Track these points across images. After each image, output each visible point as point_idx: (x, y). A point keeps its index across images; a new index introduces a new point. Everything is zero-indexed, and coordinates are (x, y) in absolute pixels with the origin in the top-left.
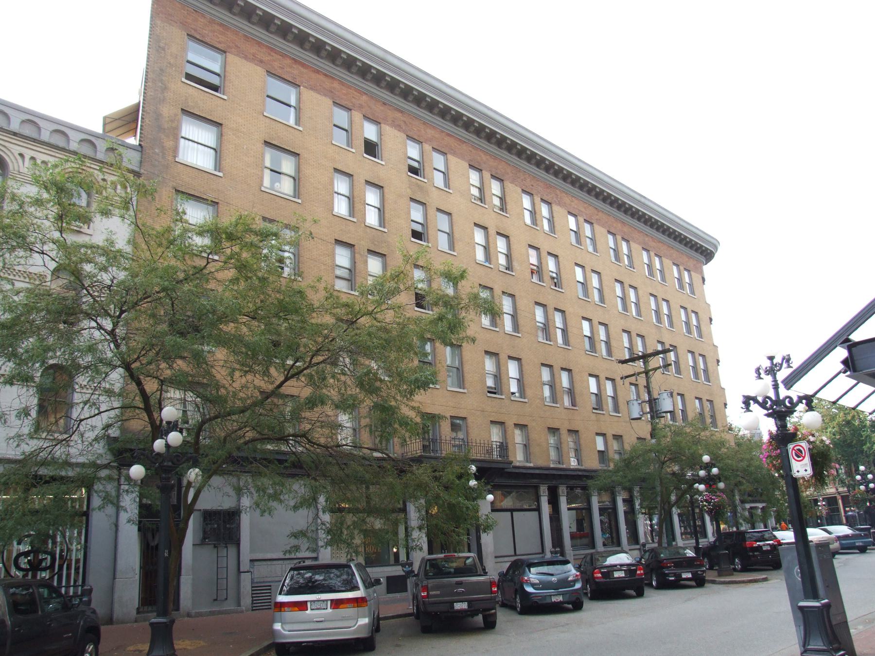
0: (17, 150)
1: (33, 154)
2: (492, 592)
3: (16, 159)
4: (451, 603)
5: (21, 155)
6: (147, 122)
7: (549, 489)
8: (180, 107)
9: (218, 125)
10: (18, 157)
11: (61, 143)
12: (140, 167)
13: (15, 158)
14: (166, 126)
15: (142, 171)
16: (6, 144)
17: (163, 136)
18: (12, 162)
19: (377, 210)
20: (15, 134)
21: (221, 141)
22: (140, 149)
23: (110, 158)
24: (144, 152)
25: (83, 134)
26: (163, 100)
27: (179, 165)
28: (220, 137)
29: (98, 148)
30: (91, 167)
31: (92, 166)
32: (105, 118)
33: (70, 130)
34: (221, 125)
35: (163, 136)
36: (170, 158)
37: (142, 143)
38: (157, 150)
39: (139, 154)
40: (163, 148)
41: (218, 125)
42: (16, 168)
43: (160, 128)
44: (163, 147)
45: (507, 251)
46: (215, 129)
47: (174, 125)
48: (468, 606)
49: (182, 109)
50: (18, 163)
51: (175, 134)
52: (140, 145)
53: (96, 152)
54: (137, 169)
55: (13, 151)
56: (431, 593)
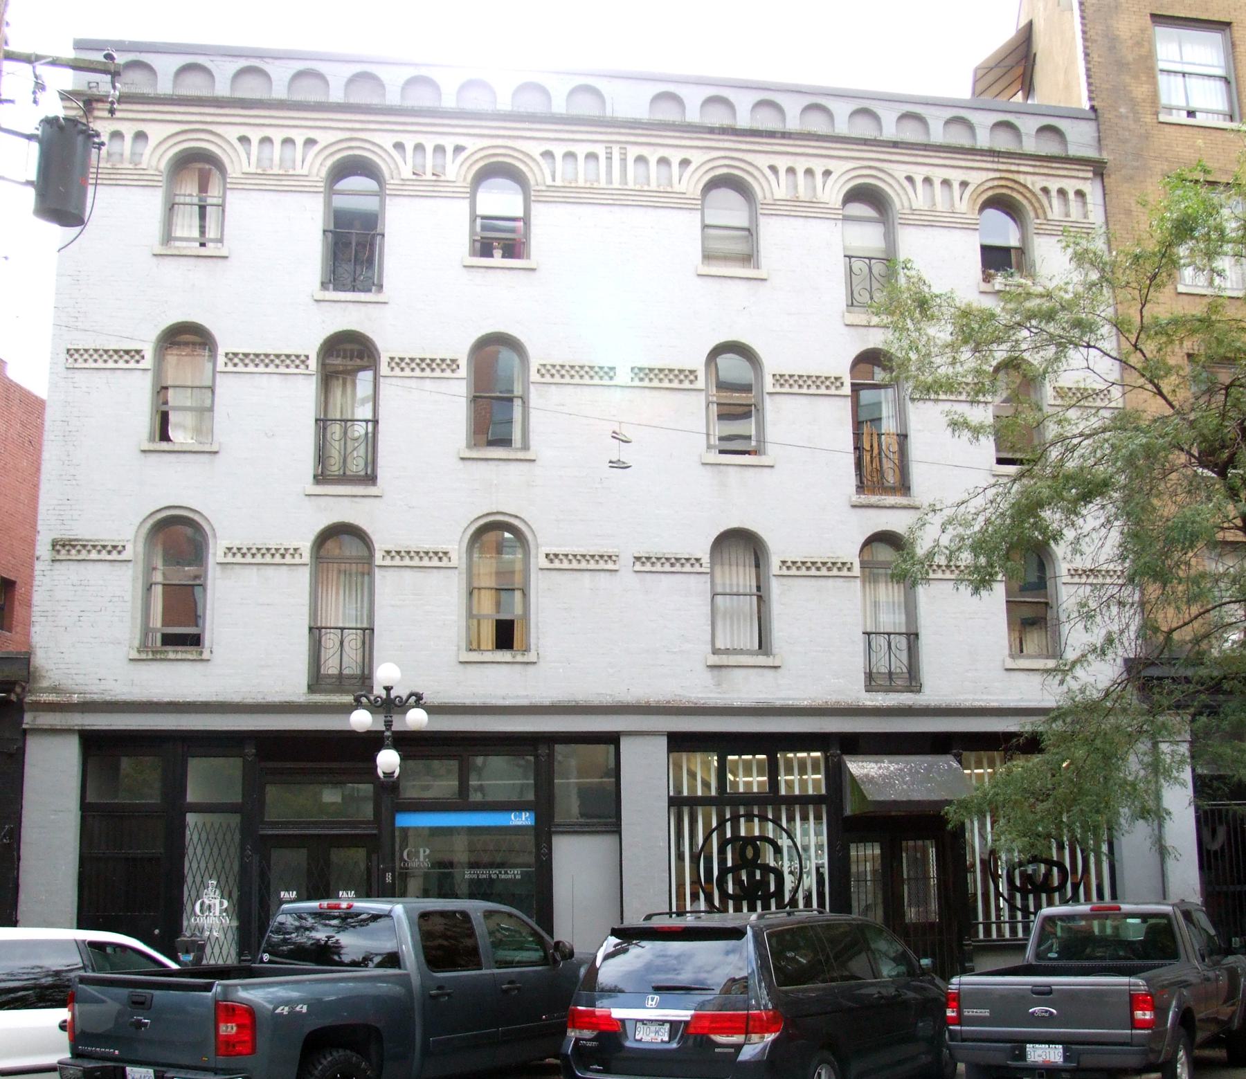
0: (900, 171)
1: (926, 171)
2: (1135, 1024)
3: (904, 189)
4: (1019, 1045)
5: (910, 179)
6: (1096, 59)
7: (988, 758)
8: (1148, 11)
9: (1223, 26)
10: (906, 184)
11: (962, 139)
12: (1100, 149)
13: (901, 185)
14: (1130, 58)
15: (1105, 156)
16: (749, 157)
17: (1128, 79)
18: (898, 194)
19: (1220, 85)
20: (895, 144)
21: (1234, 59)
22: (1092, 115)
23: (1050, 147)
24: (1101, 119)
25: (949, 109)
26: (1116, 7)
27: (1167, 128)
28: (1232, 48)
29: (1023, 129)
30: (1018, 172)
31: (1022, 169)
32: (976, 70)
33: (1058, 119)
34: (1229, 24)
35: (1128, 79)
36: (1149, 119)
37: (1095, 103)
38: (1123, 110)
39: (1092, 125)
40: (1133, 103)
41: (1223, 26)
42: (906, 204)
43: (1121, 65)
44: (1132, 100)
45: (1227, 68)
46: (1216, 37)
47: (1144, 51)
48: (1066, 1058)
49: (1153, 16)
50: (906, 193)
51: (1147, 67)
52: (1093, 108)
53: (880, 129)
54: (1091, 153)
55: (896, 174)
56: (967, 1012)
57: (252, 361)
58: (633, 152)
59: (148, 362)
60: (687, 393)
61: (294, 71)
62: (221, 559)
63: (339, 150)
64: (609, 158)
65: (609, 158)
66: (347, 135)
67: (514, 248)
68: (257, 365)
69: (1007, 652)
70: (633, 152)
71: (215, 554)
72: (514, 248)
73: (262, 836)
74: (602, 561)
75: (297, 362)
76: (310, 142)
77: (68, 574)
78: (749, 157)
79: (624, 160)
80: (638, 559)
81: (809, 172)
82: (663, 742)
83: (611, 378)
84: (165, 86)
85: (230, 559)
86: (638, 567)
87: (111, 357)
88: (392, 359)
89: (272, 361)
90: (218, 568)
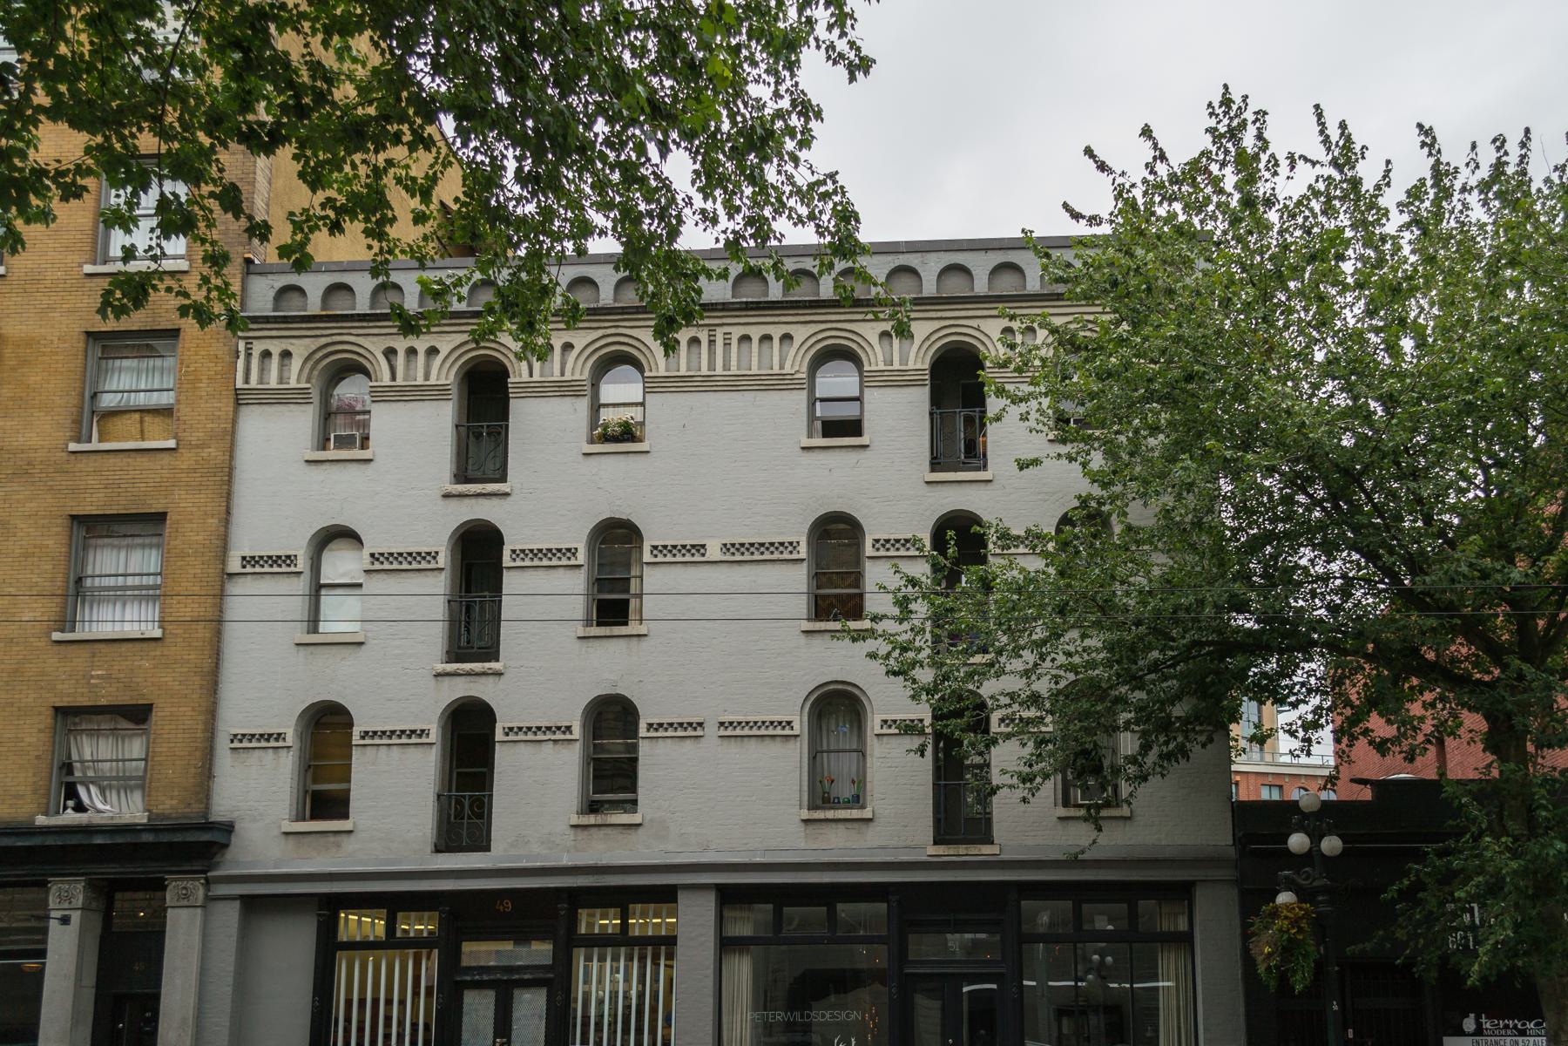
16: (360, 340)
57: (748, 549)
58: (737, 332)
59: (302, 564)
60: (714, 566)
61: (893, 266)
62: (878, 730)
63: (940, 338)
64: (712, 342)
65: (712, 342)
66: (324, 341)
67: (853, 427)
68: (752, 553)
69: (575, 809)
70: (737, 332)
71: (873, 729)
72: (853, 427)
73: (907, 974)
74: (734, 731)
75: (531, 555)
76: (787, 337)
77: (663, 749)
78: (360, 340)
79: (249, 355)
80: (722, 724)
81: (390, 353)
82: (237, 904)
83: (703, 555)
84: (981, 286)
85: (885, 731)
86: (722, 732)
87: (554, 555)
88: (877, 541)
89: (415, 558)
90: (875, 739)
